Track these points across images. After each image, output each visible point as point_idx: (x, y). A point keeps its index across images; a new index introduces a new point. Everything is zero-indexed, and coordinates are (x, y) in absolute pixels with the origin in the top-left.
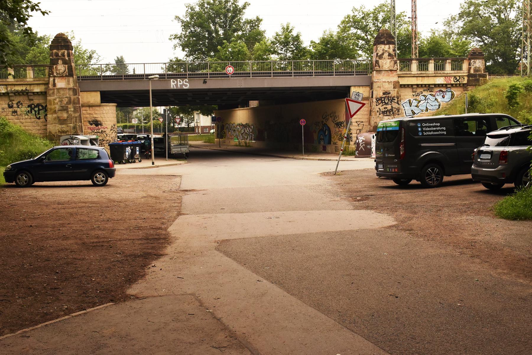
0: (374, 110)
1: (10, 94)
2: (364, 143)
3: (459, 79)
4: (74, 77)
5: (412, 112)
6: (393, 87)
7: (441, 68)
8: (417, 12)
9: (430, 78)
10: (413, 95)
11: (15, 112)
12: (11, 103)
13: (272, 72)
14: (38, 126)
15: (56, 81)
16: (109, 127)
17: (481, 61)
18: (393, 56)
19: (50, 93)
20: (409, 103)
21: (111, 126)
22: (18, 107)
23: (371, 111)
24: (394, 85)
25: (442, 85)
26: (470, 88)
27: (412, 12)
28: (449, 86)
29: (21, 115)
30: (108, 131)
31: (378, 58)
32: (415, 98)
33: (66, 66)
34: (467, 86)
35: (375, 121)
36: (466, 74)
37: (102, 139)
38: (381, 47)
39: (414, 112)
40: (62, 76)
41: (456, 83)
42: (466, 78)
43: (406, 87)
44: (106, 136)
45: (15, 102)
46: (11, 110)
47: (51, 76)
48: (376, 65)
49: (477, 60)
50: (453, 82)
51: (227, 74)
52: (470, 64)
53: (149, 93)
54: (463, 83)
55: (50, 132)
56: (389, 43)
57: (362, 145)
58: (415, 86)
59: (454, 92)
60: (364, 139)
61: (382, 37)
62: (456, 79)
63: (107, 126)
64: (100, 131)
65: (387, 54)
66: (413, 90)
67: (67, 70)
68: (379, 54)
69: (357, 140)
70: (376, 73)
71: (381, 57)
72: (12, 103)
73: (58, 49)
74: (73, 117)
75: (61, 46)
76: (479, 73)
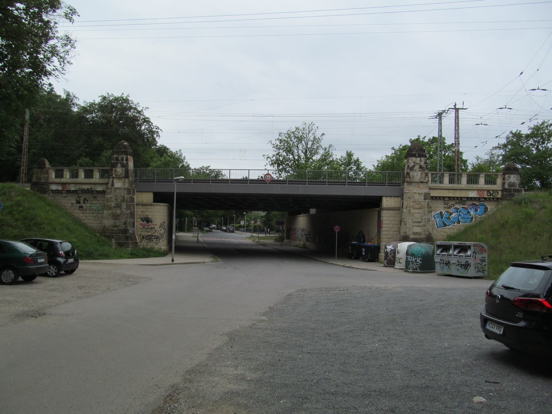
0: (404, 220)
1: (79, 192)
2: (392, 252)
3: (492, 194)
4: (130, 178)
5: (444, 224)
6: (423, 198)
7: (474, 182)
8: (460, 139)
9: (462, 191)
10: (445, 208)
11: (82, 207)
12: (78, 199)
13: (307, 180)
14: (99, 220)
15: (115, 181)
16: (159, 224)
17: (516, 176)
18: (424, 168)
19: (108, 192)
21: (160, 223)
22: (84, 203)
23: (401, 221)
24: (424, 196)
25: (475, 198)
26: (504, 202)
27: (455, 139)
28: (482, 200)
29: (85, 210)
30: (157, 228)
31: (409, 170)
32: (447, 210)
33: (124, 169)
36: (501, 189)
37: (151, 235)
38: (412, 160)
39: (445, 224)
40: (119, 178)
41: (490, 197)
42: (500, 193)
43: (438, 199)
44: (155, 232)
45: (82, 199)
46: (78, 205)
47: (111, 177)
48: (407, 176)
49: (512, 175)
51: (265, 181)
52: (504, 179)
53: (174, 195)
54: (497, 197)
55: (105, 226)
56: (420, 156)
57: (390, 254)
58: (447, 199)
59: (488, 206)
60: (393, 248)
62: (490, 193)
63: (157, 223)
64: (150, 227)
65: (418, 166)
66: (444, 202)
67: (124, 172)
68: (410, 167)
69: (386, 249)
70: (406, 184)
71: (412, 169)
72: (80, 200)
73: (118, 154)
74: (125, 214)
75: (121, 151)
76: (514, 188)
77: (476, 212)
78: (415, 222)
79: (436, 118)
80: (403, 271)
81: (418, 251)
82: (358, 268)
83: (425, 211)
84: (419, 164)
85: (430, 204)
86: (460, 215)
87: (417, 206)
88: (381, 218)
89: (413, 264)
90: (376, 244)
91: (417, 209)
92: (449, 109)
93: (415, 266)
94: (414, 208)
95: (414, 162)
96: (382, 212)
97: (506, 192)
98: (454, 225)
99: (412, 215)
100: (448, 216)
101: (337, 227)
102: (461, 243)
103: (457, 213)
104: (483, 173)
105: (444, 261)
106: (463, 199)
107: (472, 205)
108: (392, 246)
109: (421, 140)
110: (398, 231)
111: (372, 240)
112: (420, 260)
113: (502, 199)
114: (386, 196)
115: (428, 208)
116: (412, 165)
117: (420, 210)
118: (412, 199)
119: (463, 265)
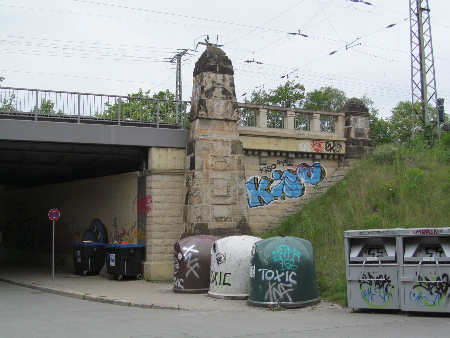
2: (197, 259)
3: (333, 147)
5: (260, 201)
9: (289, 141)
10: (261, 170)
17: (364, 119)
20: (255, 183)
24: (232, 147)
25: (308, 154)
26: (351, 162)
32: (264, 174)
34: (346, 158)
35: (199, 214)
38: (209, 77)
39: (262, 200)
41: (329, 152)
42: (344, 146)
49: (359, 117)
50: (324, 151)
52: (347, 123)
54: (339, 153)
57: (192, 265)
58: (265, 154)
59: (325, 169)
60: (197, 251)
61: (211, 60)
65: (221, 90)
66: (260, 160)
68: (206, 89)
70: (200, 123)
76: (363, 138)
77: (308, 179)
78: (217, 196)
79: (172, 61)
80: (245, 302)
81: (286, 254)
82: (130, 305)
83: (234, 175)
84: (222, 85)
85: (242, 161)
86: (284, 184)
87: (219, 166)
88: (147, 183)
89: (276, 286)
90: (135, 243)
91: (220, 171)
92: (199, 43)
93: (283, 291)
94: (215, 170)
95: (213, 82)
96: (148, 178)
97: (353, 144)
100: (266, 185)
101: (54, 211)
102: (427, 231)
103: (280, 181)
104: (318, 112)
105: (370, 276)
106: (290, 155)
107: (302, 166)
108: (193, 246)
109: (144, 94)
110: (179, 216)
111: (126, 236)
112: (293, 277)
113: (347, 156)
114: (157, 147)
115: (238, 169)
116: (208, 86)
119: (435, 284)
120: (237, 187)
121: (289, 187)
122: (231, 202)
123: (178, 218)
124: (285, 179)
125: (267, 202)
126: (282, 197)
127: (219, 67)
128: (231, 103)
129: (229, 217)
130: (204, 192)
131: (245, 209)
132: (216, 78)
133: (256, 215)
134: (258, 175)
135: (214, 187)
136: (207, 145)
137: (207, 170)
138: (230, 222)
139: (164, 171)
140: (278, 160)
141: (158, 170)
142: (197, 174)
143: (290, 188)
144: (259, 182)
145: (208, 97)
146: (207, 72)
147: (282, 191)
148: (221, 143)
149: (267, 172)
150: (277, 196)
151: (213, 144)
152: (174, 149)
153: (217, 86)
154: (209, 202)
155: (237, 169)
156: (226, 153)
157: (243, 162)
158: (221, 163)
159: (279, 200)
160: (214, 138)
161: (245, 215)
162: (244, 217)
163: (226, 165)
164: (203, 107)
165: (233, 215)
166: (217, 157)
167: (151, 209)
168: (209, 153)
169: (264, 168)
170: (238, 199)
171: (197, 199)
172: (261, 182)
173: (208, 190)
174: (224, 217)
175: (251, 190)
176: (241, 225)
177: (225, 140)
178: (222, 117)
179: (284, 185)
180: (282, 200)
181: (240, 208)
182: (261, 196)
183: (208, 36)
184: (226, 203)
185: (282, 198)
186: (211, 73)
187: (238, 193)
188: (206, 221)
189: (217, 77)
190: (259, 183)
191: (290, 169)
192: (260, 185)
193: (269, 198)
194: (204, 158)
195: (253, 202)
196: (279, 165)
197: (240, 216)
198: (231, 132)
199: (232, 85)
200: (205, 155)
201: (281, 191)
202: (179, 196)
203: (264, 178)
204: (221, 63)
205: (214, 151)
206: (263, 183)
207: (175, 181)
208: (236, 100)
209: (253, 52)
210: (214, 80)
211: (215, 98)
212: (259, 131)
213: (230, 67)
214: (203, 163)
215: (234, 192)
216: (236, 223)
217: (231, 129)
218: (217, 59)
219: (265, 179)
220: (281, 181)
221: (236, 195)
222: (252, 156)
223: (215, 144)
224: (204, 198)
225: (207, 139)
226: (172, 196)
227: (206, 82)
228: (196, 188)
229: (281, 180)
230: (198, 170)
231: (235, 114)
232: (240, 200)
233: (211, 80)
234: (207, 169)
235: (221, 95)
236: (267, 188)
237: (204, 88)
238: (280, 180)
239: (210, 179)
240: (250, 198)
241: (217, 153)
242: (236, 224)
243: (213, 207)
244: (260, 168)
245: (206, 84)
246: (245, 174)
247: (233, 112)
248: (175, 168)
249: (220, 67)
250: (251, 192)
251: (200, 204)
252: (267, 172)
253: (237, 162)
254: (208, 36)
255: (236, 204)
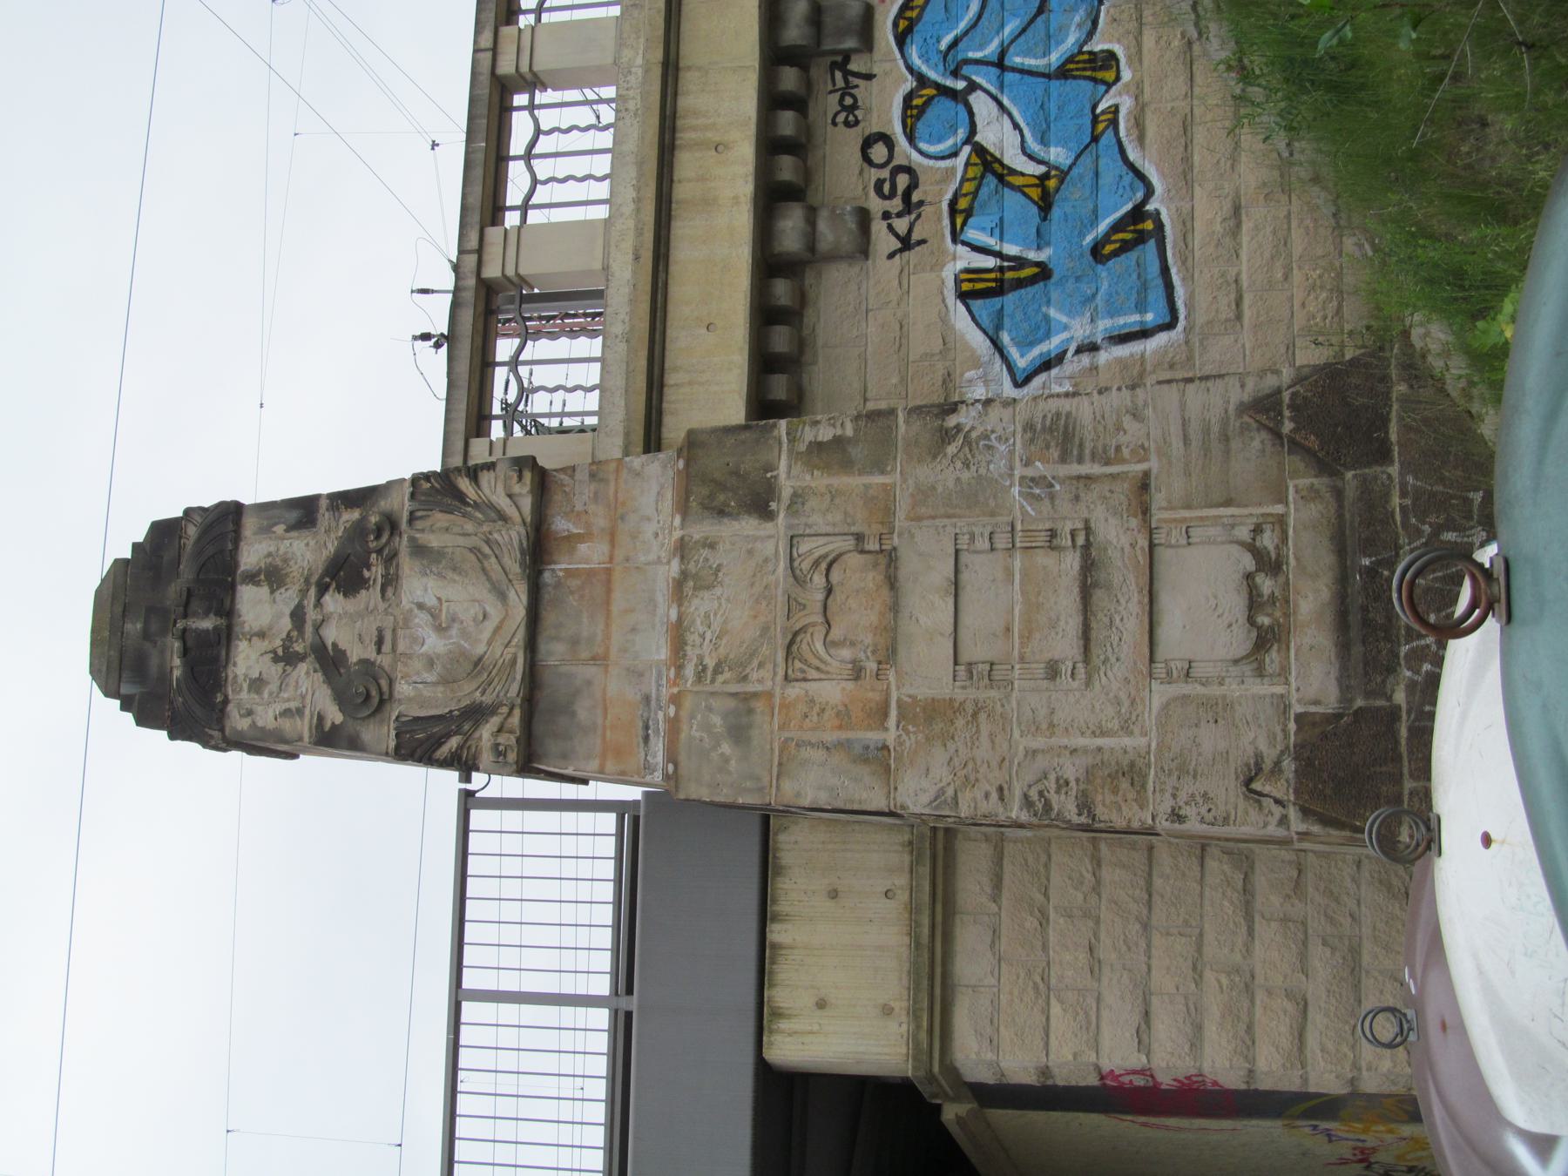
5: (1126, 247)
6: (748, 525)
9: (692, 51)
10: (906, 243)
20: (999, 289)
24: (722, 512)
32: (934, 222)
35: (1226, 790)
38: (257, 684)
39: (1117, 227)
58: (790, 229)
66: (833, 257)
68: (334, 716)
83: (924, 494)
84: (304, 593)
86: (1000, 63)
91: (895, 608)
94: (889, 654)
95: (288, 658)
98: (1139, 124)
99: (992, 673)
100: (1012, 199)
103: (979, 102)
106: (794, 33)
114: (762, 1018)
117: (909, 565)
118: (762, 679)
120: (1017, 473)
121: (1024, 30)
122: (1134, 523)
123: (1260, 881)
124: (968, 62)
125: (1133, 190)
126: (1094, 80)
127: (195, 615)
128: (419, 524)
129: (1244, 533)
130: (1054, 741)
131: (1183, 406)
132: (262, 635)
133: (1233, 272)
134: (938, 266)
135: (1022, 659)
136: (710, 709)
137: (893, 713)
138: (1284, 533)
139: (925, 983)
140: (834, 123)
141: (918, 1027)
142: (925, 798)
143: (1032, 21)
144: (990, 262)
145: (382, 702)
146: (226, 701)
147: (1047, 76)
148: (696, 602)
149: (921, 203)
150: (1088, 121)
151: (701, 658)
152: (774, 901)
153: (309, 629)
154: (1133, 702)
155: (883, 472)
156: (766, 560)
157: (832, 422)
158: (838, 596)
159: (1119, 99)
160: (664, 654)
161: (1231, 408)
162: (1243, 409)
163: (855, 560)
164: (448, 736)
165: (1228, 503)
166: (796, 634)
167: (1193, 1071)
168: (769, 695)
169: (890, 227)
170: (1107, 463)
171: (1109, 798)
172: (991, 242)
173: (1043, 712)
174: (1249, 577)
175: (1047, 318)
176: (1312, 442)
177: (675, 567)
178: (512, 595)
179: (1007, 63)
180: (1118, 79)
181: (1177, 443)
182: (1089, 239)
183: (415, 338)
184: (1143, 560)
185: (1100, 75)
186: (231, 676)
187: (1063, 459)
188: (1278, 729)
189: (256, 626)
190: (998, 255)
191: (895, 25)
192: (1011, 249)
193: (1107, 179)
194: (808, 736)
195: (1134, 297)
196: (869, 111)
197: (1235, 444)
198: (622, 518)
199: (304, 511)
200: (782, 728)
201: (1055, 84)
202: (1097, 862)
203: (964, 224)
204: (174, 591)
205: (752, 656)
206: (1000, 230)
207: (996, 898)
208: (404, 480)
209: (434, 145)
210: (274, 652)
211: (387, 647)
212: (627, 274)
213: (192, 531)
214: (840, 745)
215: (1052, 497)
216: (1295, 474)
217: (600, 521)
218: (146, 623)
219: (969, 213)
220: (979, 93)
221: (1079, 478)
222: (809, 316)
223: (701, 649)
224: (1100, 741)
225: (672, 711)
226: (1098, 922)
227: (286, 713)
228: (1028, 803)
229: (973, 87)
230: (891, 789)
231: (493, 489)
232: (1118, 448)
233: (274, 671)
234: (886, 715)
235: (369, 597)
236: (1035, 193)
237: (328, 726)
238: (972, 98)
239: (960, 695)
240: (1104, 325)
241: (765, 630)
242: (1302, 480)
243: (1169, 673)
244: (891, 256)
245: (300, 712)
246: (916, 411)
247: (476, 506)
248: (903, 896)
249: (195, 605)
250: (1064, 319)
251: (1146, 776)
252: (921, 203)
253: (827, 468)
254: (415, 338)
255: (1147, 474)
